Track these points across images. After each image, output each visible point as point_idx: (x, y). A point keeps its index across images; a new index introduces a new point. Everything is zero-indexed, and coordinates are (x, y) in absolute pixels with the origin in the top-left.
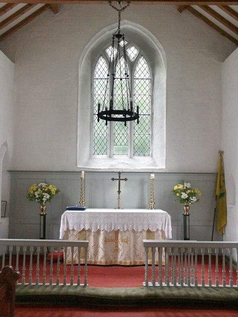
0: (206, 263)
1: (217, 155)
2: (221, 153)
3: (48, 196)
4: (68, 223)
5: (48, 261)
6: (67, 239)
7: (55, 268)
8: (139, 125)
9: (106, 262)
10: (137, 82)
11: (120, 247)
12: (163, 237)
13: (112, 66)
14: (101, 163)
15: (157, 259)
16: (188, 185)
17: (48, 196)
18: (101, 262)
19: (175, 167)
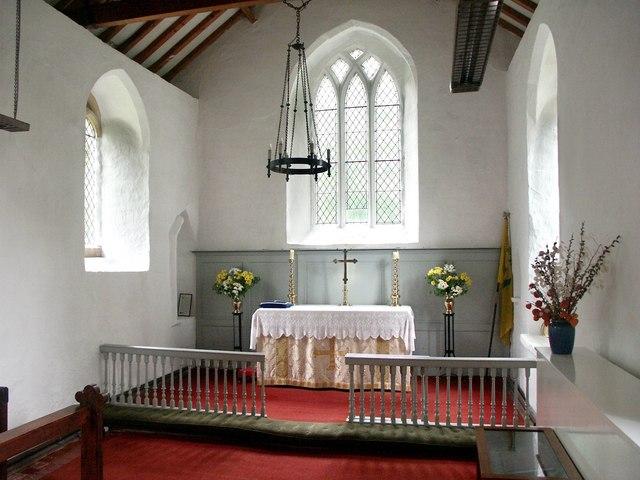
0: (465, 387)
1: (500, 219)
2: (507, 216)
3: (241, 288)
4: (261, 326)
5: (240, 379)
6: (261, 351)
7: (230, 391)
8: (330, 179)
9: (317, 384)
10: (379, 110)
11: (337, 362)
12: (403, 350)
13: (341, 90)
14: (324, 236)
15: (398, 385)
16: (450, 268)
17: (241, 288)
18: (309, 383)
19: (433, 240)
